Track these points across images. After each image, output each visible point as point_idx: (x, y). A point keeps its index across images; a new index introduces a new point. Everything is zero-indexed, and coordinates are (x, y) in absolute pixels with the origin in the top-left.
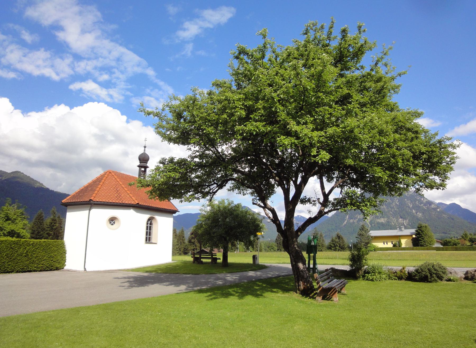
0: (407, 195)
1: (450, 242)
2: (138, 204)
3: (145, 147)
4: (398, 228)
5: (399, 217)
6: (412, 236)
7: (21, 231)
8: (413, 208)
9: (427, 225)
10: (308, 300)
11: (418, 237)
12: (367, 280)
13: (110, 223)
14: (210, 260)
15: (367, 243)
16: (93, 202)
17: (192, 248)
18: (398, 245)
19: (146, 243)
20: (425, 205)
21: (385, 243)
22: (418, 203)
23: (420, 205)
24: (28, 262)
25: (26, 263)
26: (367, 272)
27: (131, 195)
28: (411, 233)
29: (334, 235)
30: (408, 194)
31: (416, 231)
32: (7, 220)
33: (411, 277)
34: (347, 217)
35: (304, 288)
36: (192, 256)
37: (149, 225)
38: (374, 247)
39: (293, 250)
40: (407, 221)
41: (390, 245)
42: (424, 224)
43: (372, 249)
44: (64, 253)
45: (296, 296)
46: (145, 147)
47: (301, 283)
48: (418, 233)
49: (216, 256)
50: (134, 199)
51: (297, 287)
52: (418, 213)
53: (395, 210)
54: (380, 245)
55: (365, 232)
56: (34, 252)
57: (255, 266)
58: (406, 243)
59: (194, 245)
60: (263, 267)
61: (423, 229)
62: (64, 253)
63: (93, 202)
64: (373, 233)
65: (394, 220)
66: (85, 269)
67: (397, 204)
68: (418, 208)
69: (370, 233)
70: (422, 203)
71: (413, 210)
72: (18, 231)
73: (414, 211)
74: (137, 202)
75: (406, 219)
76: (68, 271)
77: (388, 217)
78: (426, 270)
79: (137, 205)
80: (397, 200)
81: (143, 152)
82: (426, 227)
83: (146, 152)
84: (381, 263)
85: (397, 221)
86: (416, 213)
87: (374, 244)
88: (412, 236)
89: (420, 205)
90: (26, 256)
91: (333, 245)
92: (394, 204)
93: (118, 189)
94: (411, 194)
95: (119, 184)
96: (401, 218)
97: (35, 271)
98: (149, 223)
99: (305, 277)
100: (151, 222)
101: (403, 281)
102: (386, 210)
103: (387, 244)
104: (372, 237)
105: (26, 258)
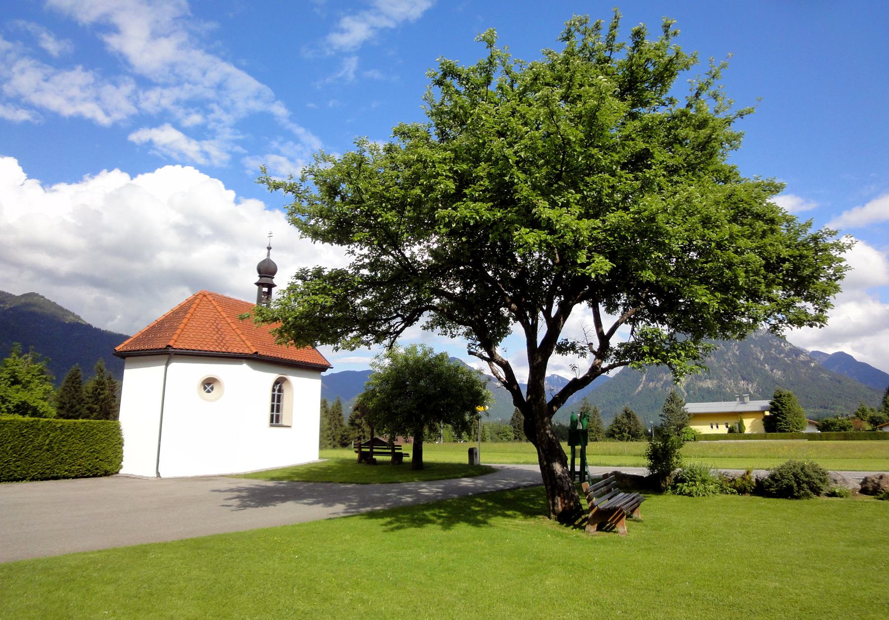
0: (754, 337)
1: (833, 424)
2: (256, 353)
3: (269, 248)
4: (738, 399)
5: (740, 377)
6: (763, 412)
7: (40, 403)
8: (766, 360)
9: (791, 392)
10: (570, 531)
11: (776, 415)
12: (681, 494)
13: (205, 388)
14: (389, 458)
15: (681, 426)
16: (173, 350)
17: (357, 435)
18: (737, 430)
19: (271, 426)
20: (788, 355)
21: (714, 427)
22: (775, 351)
23: (778, 356)
24: (53, 461)
25: (49, 462)
26: (680, 480)
27: (244, 339)
28: (763, 407)
29: (619, 411)
30: (756, 336)
31: (772, 403)
32: (13, 383)
33: (761, 489)
34: (644, 377)
35: (564, 509)
36: (357, 450)
37: (276, 393)
38: (693, 432)
39: (543, 439)
40: (755, 385)
41: (723, 430)
42: (785, 392)
43: (690, 436)
44: (120, 444)
45: (548, 524)
46: (269, 248)
47: (558, 500)
48: (774, 408)
49: (401, 449)
50: (249, 344)
51: (551, 508)
52: (775, 371)
53: (732, 365)
54: (704, 429)
55: (677, 405)
56: (64, 443)
57: (473, 469)
58: (753, 426)
59: (360, 430)
60: (487, 471)
61: (784, 400)
62: (120, 444)
63: (173, 350)
64: (692, 408)
65: (731, 384)
66: (158, 473)
67: (736, 355)
68: (774, 362)
69: (685, 407)
70: (781, 351)
71: (766, 365)
72: (35, 405)
73: (767, 367)
74: (255, 351)
75: (752, 382)
76: (127, 477)
77: (720, 379)
78: (790, 476)
79: (255, 356)
80: (736, 347)
81: (265, 257)
82: (789, 396)
83: (272, 258)
84: (707, 463)
85: (736, 385)
86: (772, 371)
87: (693, 427)
88: (763, 412)
89: (778, 356)
90: (48, 450)
91: (617, 430)
92: (730, 354)
93: (219, 327)
94: (762, 334)
95: (221, 317)
96: (744, 379)
97: (65, 477)
98: (277, 388)
99: (566, 489)
100: (280, 387)
101: (747, 497)
102: (716, 365)
103: (717, 427)
104: (689, 415)
105: (49, 454)
